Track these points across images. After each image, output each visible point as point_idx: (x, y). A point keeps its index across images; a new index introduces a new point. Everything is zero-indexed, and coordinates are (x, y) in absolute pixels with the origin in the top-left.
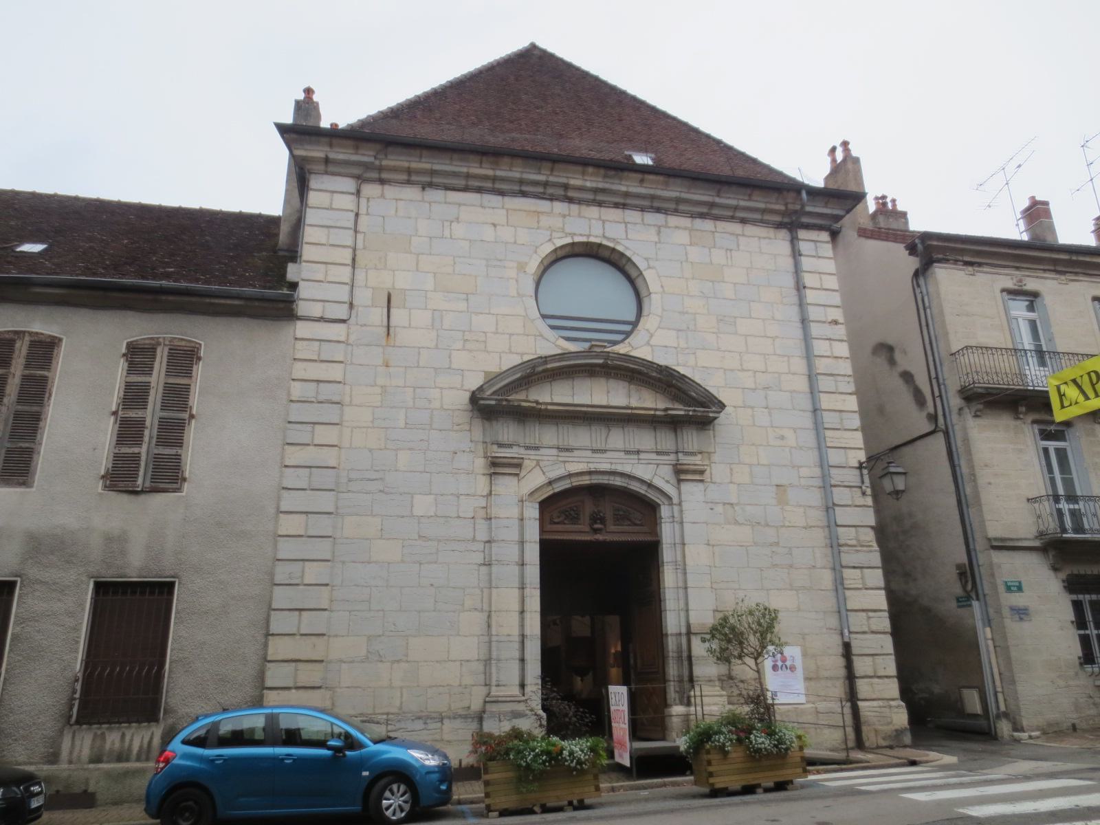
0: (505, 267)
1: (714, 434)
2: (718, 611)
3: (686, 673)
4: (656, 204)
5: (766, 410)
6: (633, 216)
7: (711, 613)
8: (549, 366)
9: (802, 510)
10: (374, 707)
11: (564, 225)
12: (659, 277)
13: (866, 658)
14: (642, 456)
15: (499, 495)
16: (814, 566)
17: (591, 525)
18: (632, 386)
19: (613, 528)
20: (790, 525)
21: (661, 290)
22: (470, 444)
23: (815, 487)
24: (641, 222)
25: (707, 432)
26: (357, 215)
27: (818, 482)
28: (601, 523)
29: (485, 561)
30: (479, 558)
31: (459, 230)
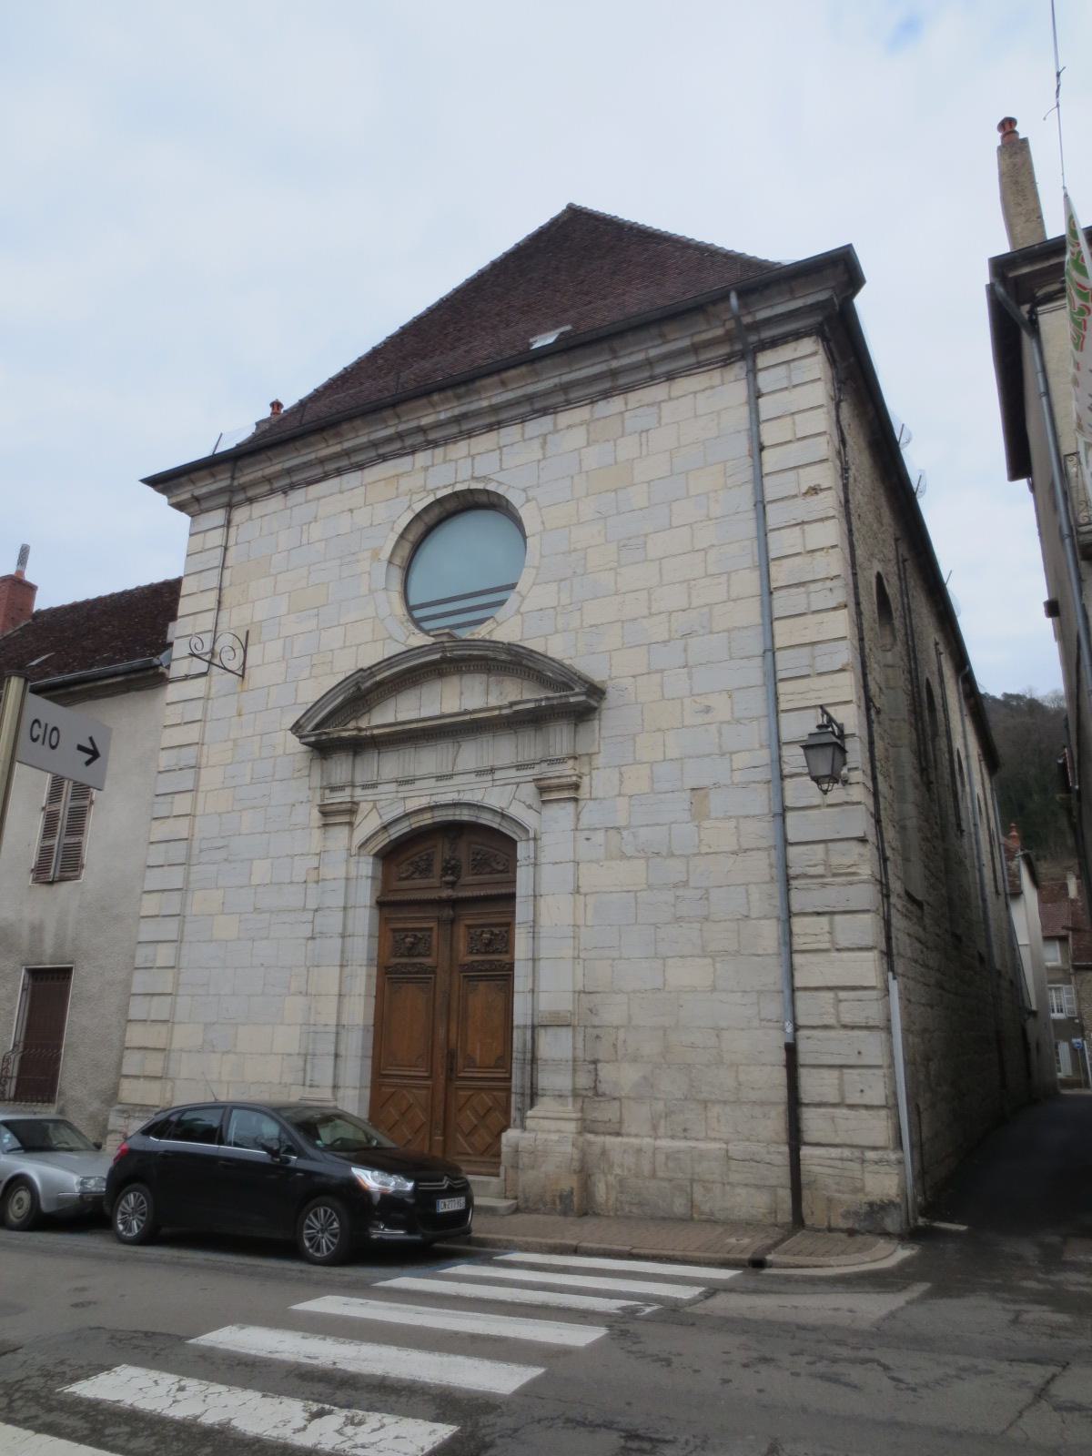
1: (600, 725)
2: (584, 992)
4: (537, 406)
6: (510, 434)
8: (378, 678)
9: (733, 823)
13: (825, 1073)
14: (498, 775)
16: (747, 917)
18: (492, 679)
20: (708, 850)
23: (758, 782)
25: (590, 723)
27: (765, 774)
30: (306, 930)
31: (316, 531)
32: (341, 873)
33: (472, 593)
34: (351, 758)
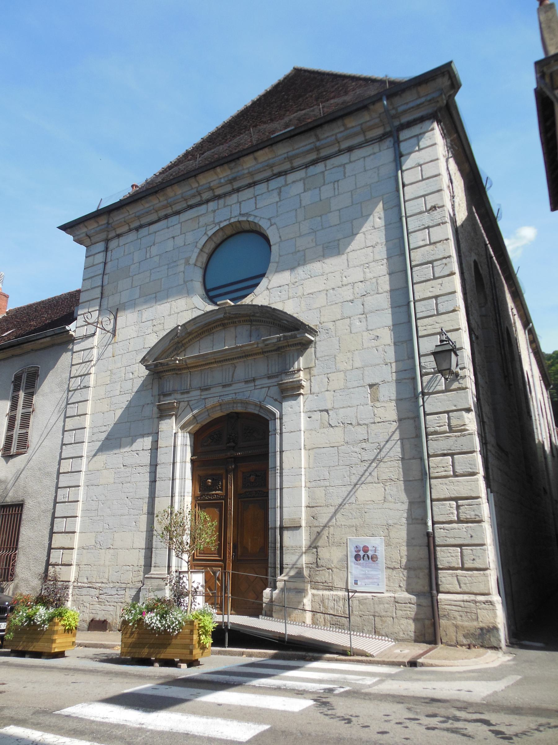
26: (105, 263)
31: (154, 250)
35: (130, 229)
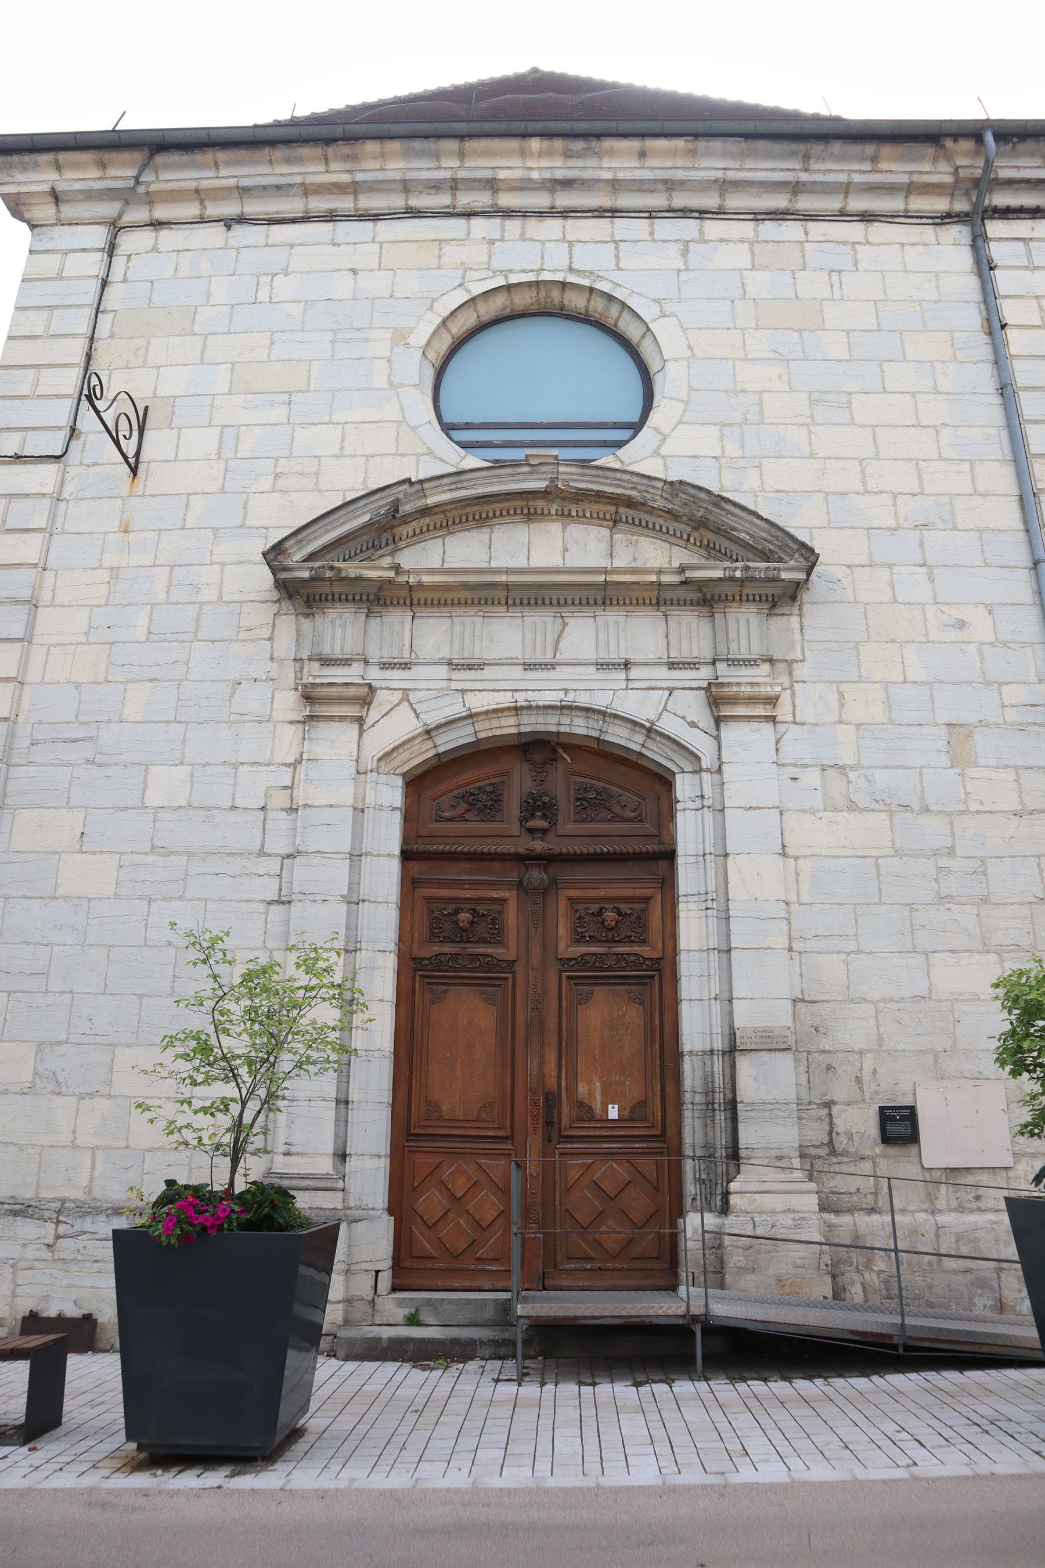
0: (367, 340)
2: (803, 1001)
3: (721, 1139)
5: (923, 570)
7: (789, 1005)
9: (1011, 775)
10: (38, 1187)
11: (490, 258)
12: (684, 330)
15: (317, 760)
17: (523, 821)
19: (572, 828)
21: (688, 353)
22: (270, 663)
24: (648, 238)
26: (105, 283)
28: (544, 817)
29: (280, 896)
31: (285, 288)
32: (346, 794)
33: (586, 423)
34: (363, 617)
35: (201, 216)
